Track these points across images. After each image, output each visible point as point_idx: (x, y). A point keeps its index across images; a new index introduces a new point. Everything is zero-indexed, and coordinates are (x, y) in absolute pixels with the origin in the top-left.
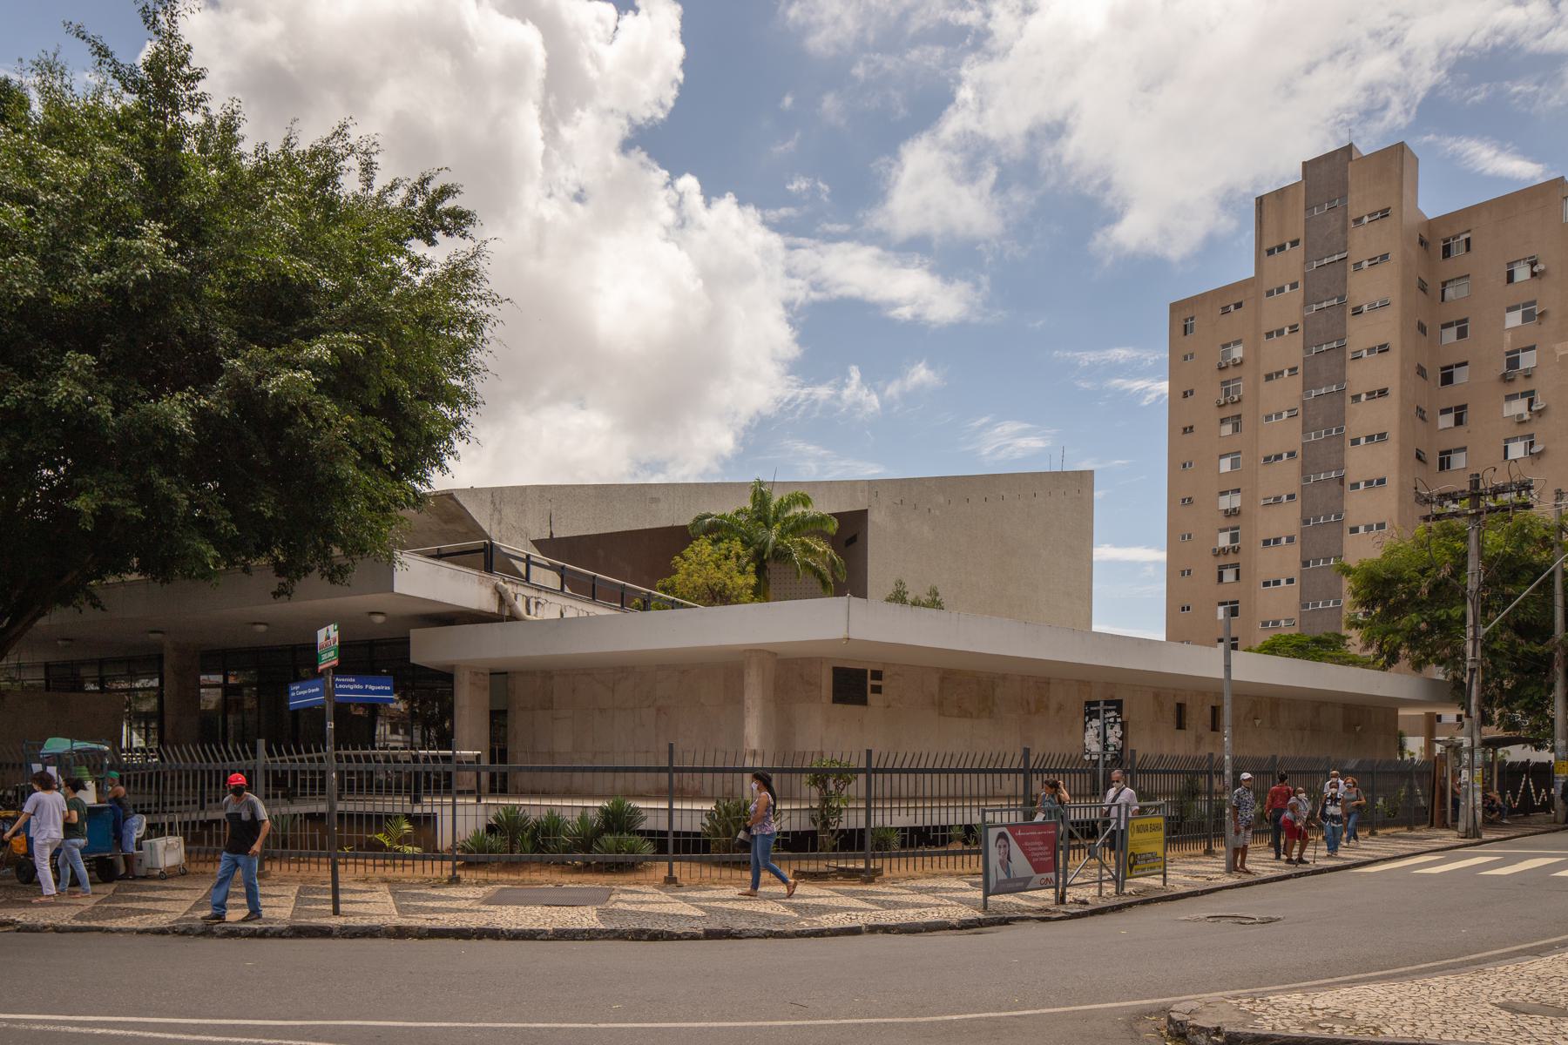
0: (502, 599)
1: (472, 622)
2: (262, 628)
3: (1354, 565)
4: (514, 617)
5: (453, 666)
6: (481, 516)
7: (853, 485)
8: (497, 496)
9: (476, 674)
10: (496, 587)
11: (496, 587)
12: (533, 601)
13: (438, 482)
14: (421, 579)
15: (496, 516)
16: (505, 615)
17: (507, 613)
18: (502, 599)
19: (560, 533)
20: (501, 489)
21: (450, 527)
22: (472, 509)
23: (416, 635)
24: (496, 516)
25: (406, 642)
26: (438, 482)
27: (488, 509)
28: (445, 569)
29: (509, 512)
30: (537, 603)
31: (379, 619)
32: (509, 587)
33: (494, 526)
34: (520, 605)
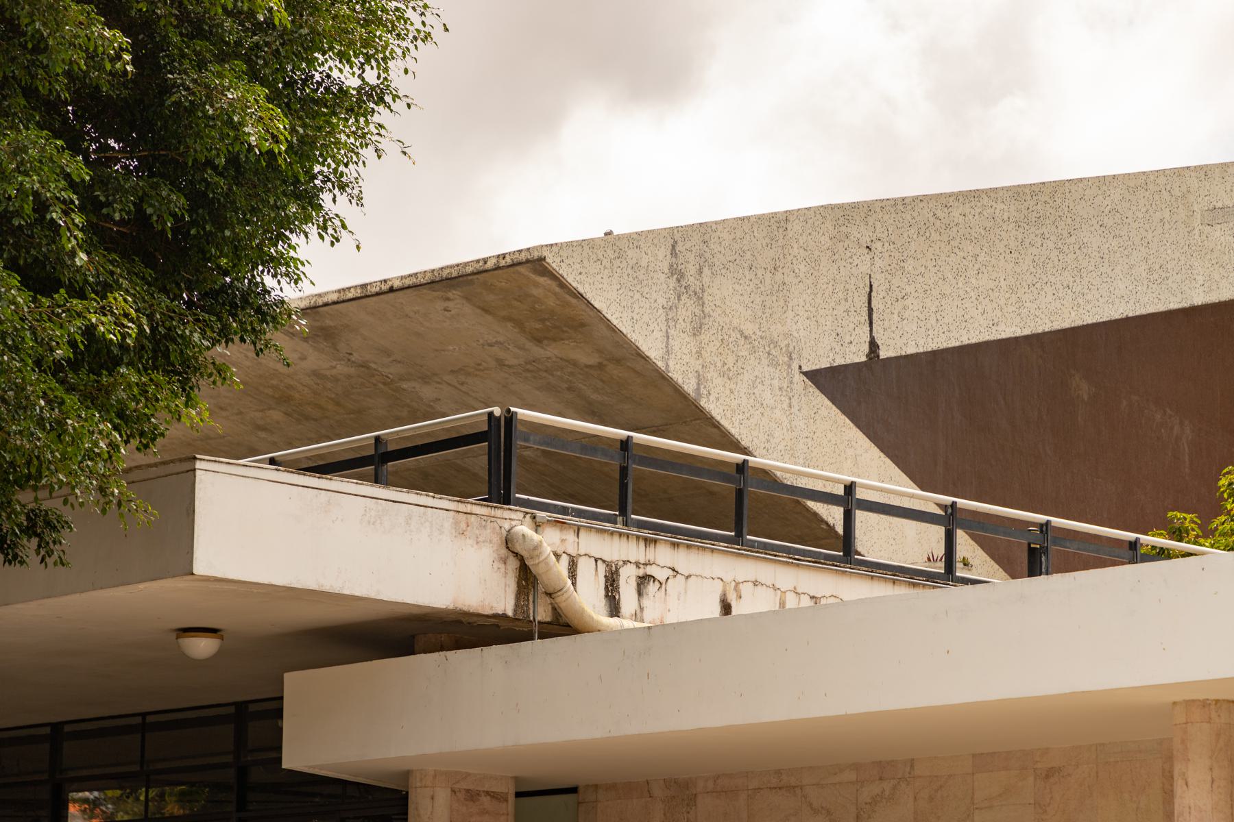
0: (527, 579)
1: (460, 644)
3: (29, 490)
4: (563, 625)
5: (406, 775)
8: (686, 255)
9: (472, 796)
10: (508, 542)
11: (508, 542)
12: (627, 578)
13: (321, 267)
15: (687, 308)
16: (535, 619)
17: (543, 614)
18: (527, 579)
19: (903, 339)
21: (551, 351)
22: (605, 295)
23: (298, 687)
24: (687, 308)
25: (273, 710)
27: (661, 290)
28: (352, 499)
29: (730, 297)
30: (644, 580)
31: (202, 647)
33: (682, 343)
34: (587, 597)
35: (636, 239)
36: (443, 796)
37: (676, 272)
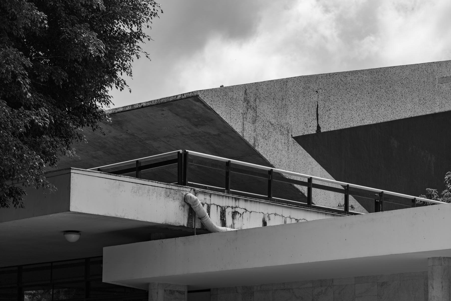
0: (192, 212)
2: (73, 238)
4: (205, 229)
5: (148, 284)
6: (234, 120)
7: (174, 96)
9: (172, 292)
10: (186, 200)
11: (186, 200)
12: (229, 212)
13: (117, 99)
14: (98, 195)
15: (250, 114)
16: (196, 226)
17: (198, 226)
18: (192, 212)
19: (328, 126)
20: (257, 85)
21: (201, 129)
22: (221, 110)
24: (250, 114)
26: (117, 99)
27: (241, 107)
28: (128, 186)
29: (266, 110)
30: (234, 214)
31: (73, 238)
32: (200, 199)
33: (249, 127)
34: (214, 219)
35: (231, 89)
36: (161, 292)
37: (246, 101)
